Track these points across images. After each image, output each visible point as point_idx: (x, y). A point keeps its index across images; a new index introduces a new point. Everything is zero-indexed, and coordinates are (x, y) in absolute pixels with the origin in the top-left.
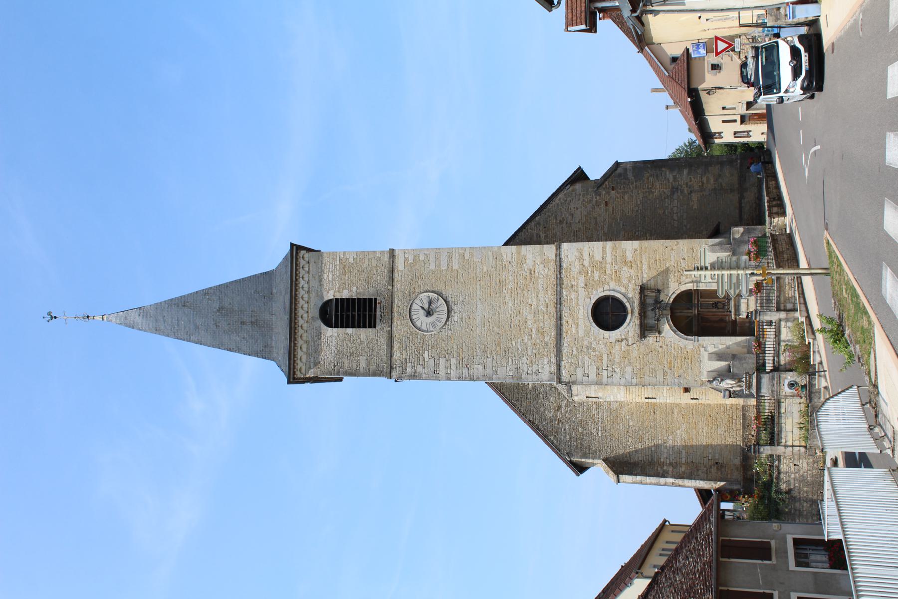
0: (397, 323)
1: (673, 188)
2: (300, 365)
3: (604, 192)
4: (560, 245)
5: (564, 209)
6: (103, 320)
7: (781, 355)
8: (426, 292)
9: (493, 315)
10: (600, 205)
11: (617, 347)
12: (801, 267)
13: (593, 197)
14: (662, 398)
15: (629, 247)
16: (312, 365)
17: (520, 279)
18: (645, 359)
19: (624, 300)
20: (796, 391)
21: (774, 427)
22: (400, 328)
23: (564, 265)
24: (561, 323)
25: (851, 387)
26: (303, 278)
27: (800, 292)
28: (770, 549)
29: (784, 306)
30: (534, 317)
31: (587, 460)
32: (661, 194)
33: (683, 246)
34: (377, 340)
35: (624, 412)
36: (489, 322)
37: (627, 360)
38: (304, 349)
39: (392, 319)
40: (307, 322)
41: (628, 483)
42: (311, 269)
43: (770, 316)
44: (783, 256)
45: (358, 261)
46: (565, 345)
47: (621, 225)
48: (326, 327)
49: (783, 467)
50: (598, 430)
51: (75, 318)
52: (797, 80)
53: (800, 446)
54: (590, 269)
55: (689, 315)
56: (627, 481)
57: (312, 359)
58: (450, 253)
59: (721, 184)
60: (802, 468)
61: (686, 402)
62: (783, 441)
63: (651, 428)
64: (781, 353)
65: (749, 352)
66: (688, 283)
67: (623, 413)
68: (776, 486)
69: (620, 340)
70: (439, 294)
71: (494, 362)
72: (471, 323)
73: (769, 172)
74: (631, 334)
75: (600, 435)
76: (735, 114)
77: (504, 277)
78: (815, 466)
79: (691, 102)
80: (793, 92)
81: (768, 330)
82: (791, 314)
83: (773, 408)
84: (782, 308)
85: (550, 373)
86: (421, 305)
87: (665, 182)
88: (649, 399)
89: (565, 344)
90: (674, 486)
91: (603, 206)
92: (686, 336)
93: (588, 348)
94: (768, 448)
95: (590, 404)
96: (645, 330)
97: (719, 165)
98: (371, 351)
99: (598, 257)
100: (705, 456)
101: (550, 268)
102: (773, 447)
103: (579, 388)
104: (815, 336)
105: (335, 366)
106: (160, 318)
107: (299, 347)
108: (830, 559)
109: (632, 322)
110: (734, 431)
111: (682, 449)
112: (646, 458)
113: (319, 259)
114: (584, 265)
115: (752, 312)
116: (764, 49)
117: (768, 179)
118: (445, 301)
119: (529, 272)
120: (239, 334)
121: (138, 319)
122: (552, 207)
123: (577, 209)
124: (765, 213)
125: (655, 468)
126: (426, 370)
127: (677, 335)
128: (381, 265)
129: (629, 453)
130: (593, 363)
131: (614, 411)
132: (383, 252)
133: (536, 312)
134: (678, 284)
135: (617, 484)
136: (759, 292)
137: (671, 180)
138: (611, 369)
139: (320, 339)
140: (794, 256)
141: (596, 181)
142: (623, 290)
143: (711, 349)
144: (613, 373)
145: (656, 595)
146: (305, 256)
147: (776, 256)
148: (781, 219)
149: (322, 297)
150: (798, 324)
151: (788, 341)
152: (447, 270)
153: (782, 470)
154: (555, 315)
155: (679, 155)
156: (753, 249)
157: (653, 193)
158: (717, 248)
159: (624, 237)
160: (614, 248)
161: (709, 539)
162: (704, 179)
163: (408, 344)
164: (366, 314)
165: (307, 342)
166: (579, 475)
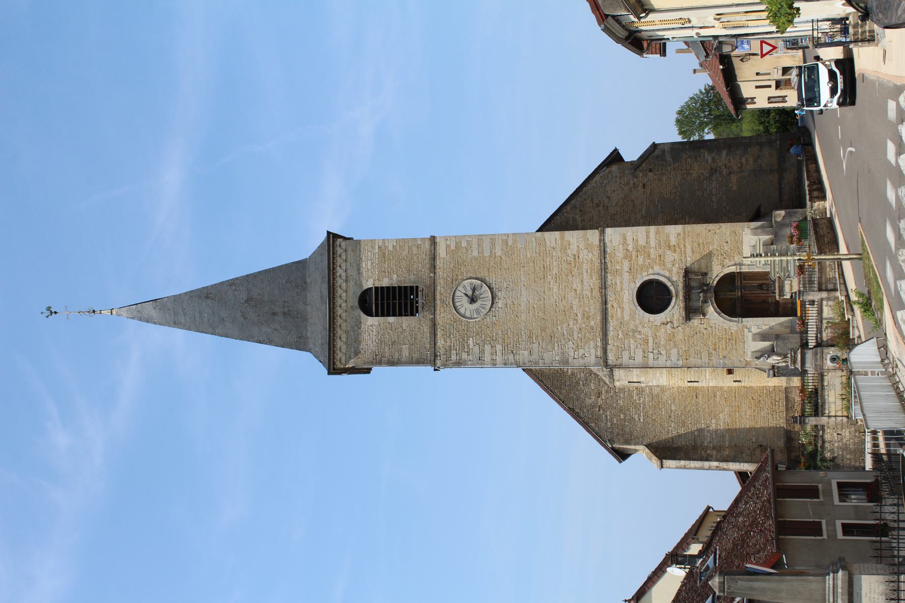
0: (440, 310)
1: (711, 169)
2: (340, 355)
3: (641, 174)
4: (604, 230)
5: (600, 192)
6: (112, 314)
7: (823, 332)
8: (470, 279)
9: (538, 300)
10: (638, 188)
11: (663, 330)
12: (841, 252)
13: (629, 179)
14: (704, 381)
15: (673, 231)
16: (352, 355)
17: (565, 265)
18: (690, 341)
19: (669, 284)
20: (838, 364)
21: (818, 399)
22: (443, 316)
23: (608, 250)
24: (606, 308)
25: (872, 338)
26: (340, 266)
27: (840, 273)
28: (818, 490)
29: (826, 286)
30: (579, 301)
31: (629, 447)
32: (699, 176)
33: (725, 229)
34: (419, 328)
35: (666, 396)
36: (534, 307)
37: (672, 342)
38: (344, 339)
39: (435, 306)
40: (346, 311)
41: (672, 468)
42: (349, 257)
43: (813, 295)
44: (824, 240)
45: (398, 249)
46: (611, 328)
47: (660, 208)
48: (366, 316)
49: (827, 437)
50: (639, 415)
51: (79, 313)
52: (833, 97)
53: (842, 416)
54: (633, 253)
55: (733, 297)
56: (671, 466)
57: (352, 348)
58: (493, 239)
59: (760, 165)
60: (845, 437)
61: (729, 386)
62: (827, 412)
63: (694, 412)
64: (823, 330)
65: (793, 331)
66: (731, 266)
67: (665, 398)
68: (821, 455)
69: (665, 323)
70: (483, 280)
71: (540, 347)
72: (516, 309)
73: (809, 154)
74: (676, 317)
75: (642, 421)
76: (769, 80)
77: (548, 263)
78: (857, 434)
79: (723, 70)
80: (830, 107)
81: (810, 309)
82: (832, 294)
83: (817, 381)
84: (824, 288)
85: (596, 357)
86: (465, 292)
87: (703, 163)
88: (692, 383)
89: (611, 328)
90: (719, 470)
91: (640, 188)
92: (730, 318)
93: (634, 331)
94: (813, 418)
95: (631, 389)
96: (691, 312)
97: (759, 146)
98: (413, 339)
99: (642, 242)
100: (749, 439)
101: (594, 253)
102: (818, 418)
103: (621, 373)
104: (854, 313)
105: (376, 355)
106: (180, 311)
107: (338, 337)
108: (868, 496)
109: (676, 306)
110: (777, 413)
111: (726, 433)
112: (689, 443)
113: (356, 247)
114: (627, 250)
115: (795, 293)
116: (806, 69)
117: (808, 163)
118: (489, 287)
119: (573, 257)
120: (270, 326)
121: (154, 313)
122: (588, 190)
123: (614, 191)
124: (805, 196)
125: (699, 452)
126: (471, 357)
127: (721, 316)
128: (422, 252)
129: (672, 438)
130: (639, 346)
131: (656, 396)
132: (423, 239)
133: (581, 297)
134: (721, 267)
135: (661, 470)
136: (802, 273)
137: (710, 161)
138: (657, 351)
139: (360, 328)
140: (834, 240)
141: (632, 163)
142: (667, 274)
143: (755, 330)
144: (659, 356)
145: (720, 538)
146: (342, 244)
147: (818, 239)
148: (822, 203)
149: (361, 286)
150: (838, 303)
151: (830, 318)
152: (490, 256)
153: (827, 440)
154: (600, 300)
155: (694, 104)
156: (795, 233)
157: (691, 174)
158: (759, 231)
159: (662, 220)
160: (657, 233)
161: (766, 483)
162: (743, 160)
163: (452, 331)
164: (390, 303)
165: (347, 332)
166: (621, 462)
